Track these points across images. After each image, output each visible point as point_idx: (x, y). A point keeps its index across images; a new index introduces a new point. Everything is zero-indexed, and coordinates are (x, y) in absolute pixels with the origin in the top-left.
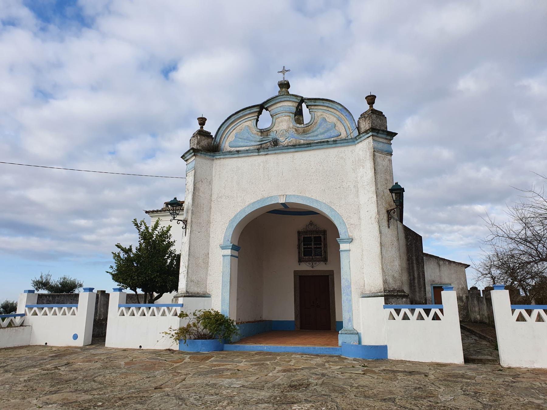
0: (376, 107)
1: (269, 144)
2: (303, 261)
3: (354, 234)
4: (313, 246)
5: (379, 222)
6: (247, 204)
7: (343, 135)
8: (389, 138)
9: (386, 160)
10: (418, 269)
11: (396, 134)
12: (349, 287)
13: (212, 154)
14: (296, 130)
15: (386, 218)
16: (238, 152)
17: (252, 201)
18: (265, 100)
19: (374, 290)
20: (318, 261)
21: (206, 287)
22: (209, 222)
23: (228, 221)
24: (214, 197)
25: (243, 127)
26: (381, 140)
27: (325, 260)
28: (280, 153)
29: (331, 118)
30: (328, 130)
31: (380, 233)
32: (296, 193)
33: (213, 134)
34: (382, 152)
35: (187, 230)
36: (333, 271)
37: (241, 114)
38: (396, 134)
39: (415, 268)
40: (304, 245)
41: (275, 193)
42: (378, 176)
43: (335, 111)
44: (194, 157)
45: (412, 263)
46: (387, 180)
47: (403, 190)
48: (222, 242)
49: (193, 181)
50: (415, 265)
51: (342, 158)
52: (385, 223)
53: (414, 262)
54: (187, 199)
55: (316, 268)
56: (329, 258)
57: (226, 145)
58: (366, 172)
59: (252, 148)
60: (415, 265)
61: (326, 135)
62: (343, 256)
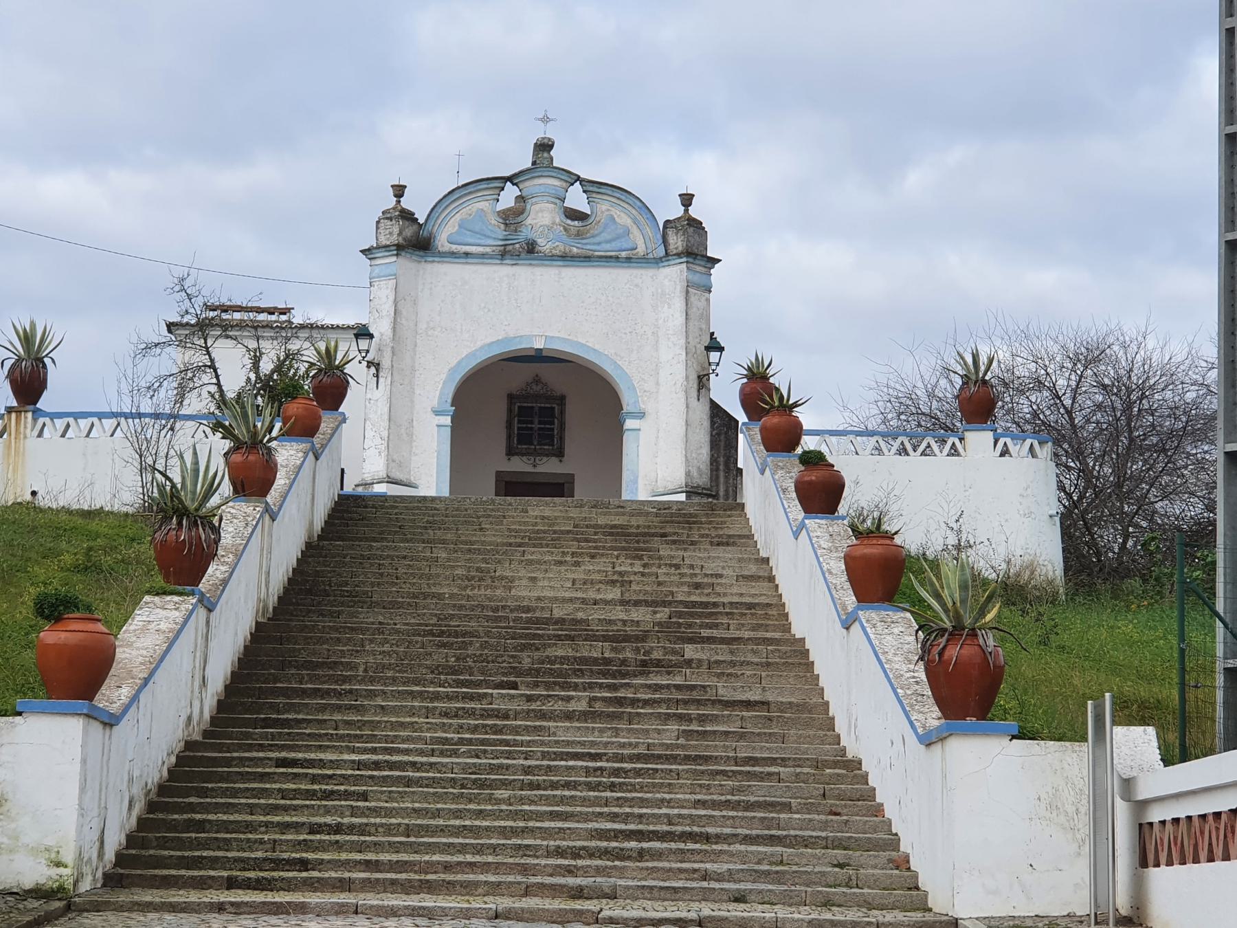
0: (694, 212)
1: (519, 249)
2: (517, 454)
3: (647, 405)
4: (536, 426)
5: (686, 392)
6: (479, 344)
7: (641, 250)
8: (709, 265)
9: (703, 299)
10: (726, 482)
11: (719, 261)
12: (636, 482)
13: (421, 253)
14: (565, 229)
15: (695, 386)
16: (467, 254)
17: (489, 340)
18: (516, 171)
19: (671, 487)
20: (547, 455)
21: (409, 472)
22: (413, 370)
23: (446, 370)
24: (422, 326)
25: (474, 210)
26: (698, 268)
27: (560, 454)
28: (537, 265)
29: (623, 219)
30: (618, 238)
31: (687, 407)
32: (562, 335)
33: (421, 221)
34: (698, 286)
35: (381, 380)
36: (573, 475)
37: (471, 188)
38: (719, 261)
39: (722, 479)
40: (519, 422)
41: (525, 332)
42: (691, 324)
43: (630, 208)
44: (394, 259)
45: (717, 470)
46: (701, 329)
47: (841, 487)
48: (435, 403)
49: (392, 298)
50: (722, 474)
51: (637, 286)
52: (694, 393)
53: (721, 467)
54: (382, 328)
55: (539, 469)
56: (568, 450)
57: (442, 241)
58: (673, 315)
59: (488, 250)
60: (722, 474)
61: (613, 244)
62: (628, 439)
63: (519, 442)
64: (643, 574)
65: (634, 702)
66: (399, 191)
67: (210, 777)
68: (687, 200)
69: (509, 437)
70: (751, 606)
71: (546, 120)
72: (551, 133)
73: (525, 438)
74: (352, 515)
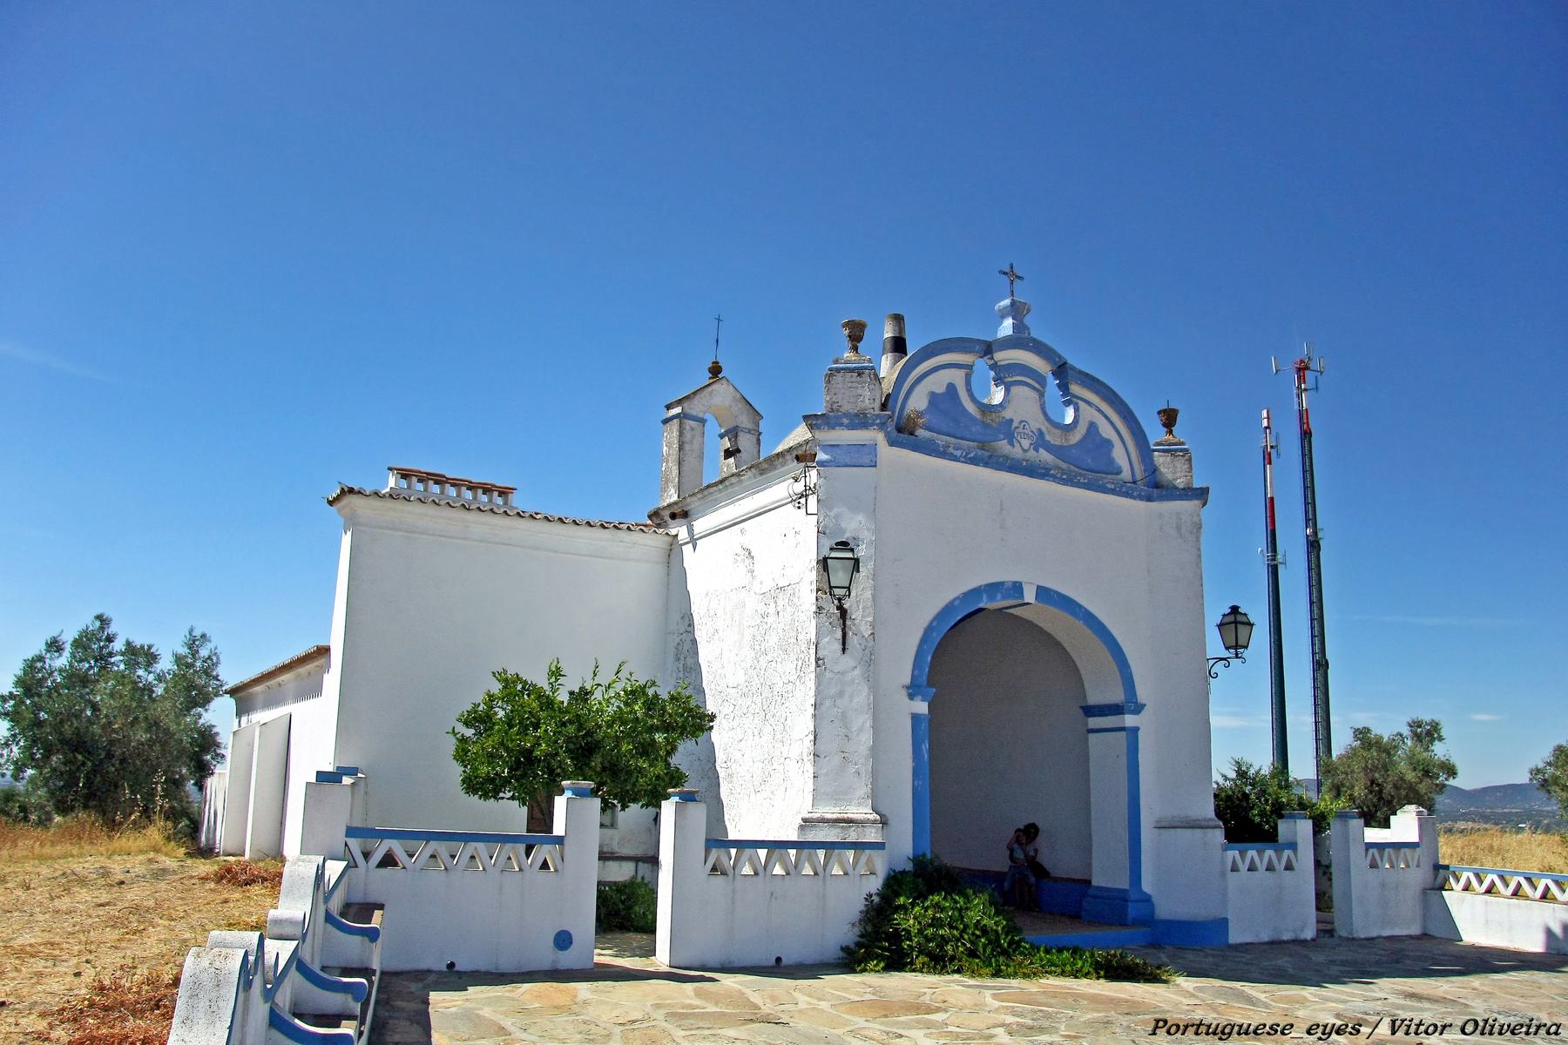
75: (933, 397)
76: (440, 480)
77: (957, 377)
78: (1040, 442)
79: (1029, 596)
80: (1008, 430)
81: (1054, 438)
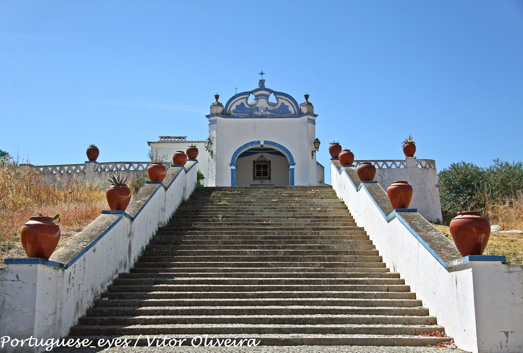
63: (257, 175)
64: (300, 208)
65: (302, 253)
66: (217, 97)
67: (126, 290)
68: (307, 97)
69: (254, 174)
70: (341, 217)
71: (262, 74)
72: (264, 77)
73: (259, 174)
74: (201, 193)
75: (237, 106)
76: (169, 137)
77: (244, 101)
78: (267, 110)
79: (262, 143)
80: (257, 109)
81: (271, 108)
